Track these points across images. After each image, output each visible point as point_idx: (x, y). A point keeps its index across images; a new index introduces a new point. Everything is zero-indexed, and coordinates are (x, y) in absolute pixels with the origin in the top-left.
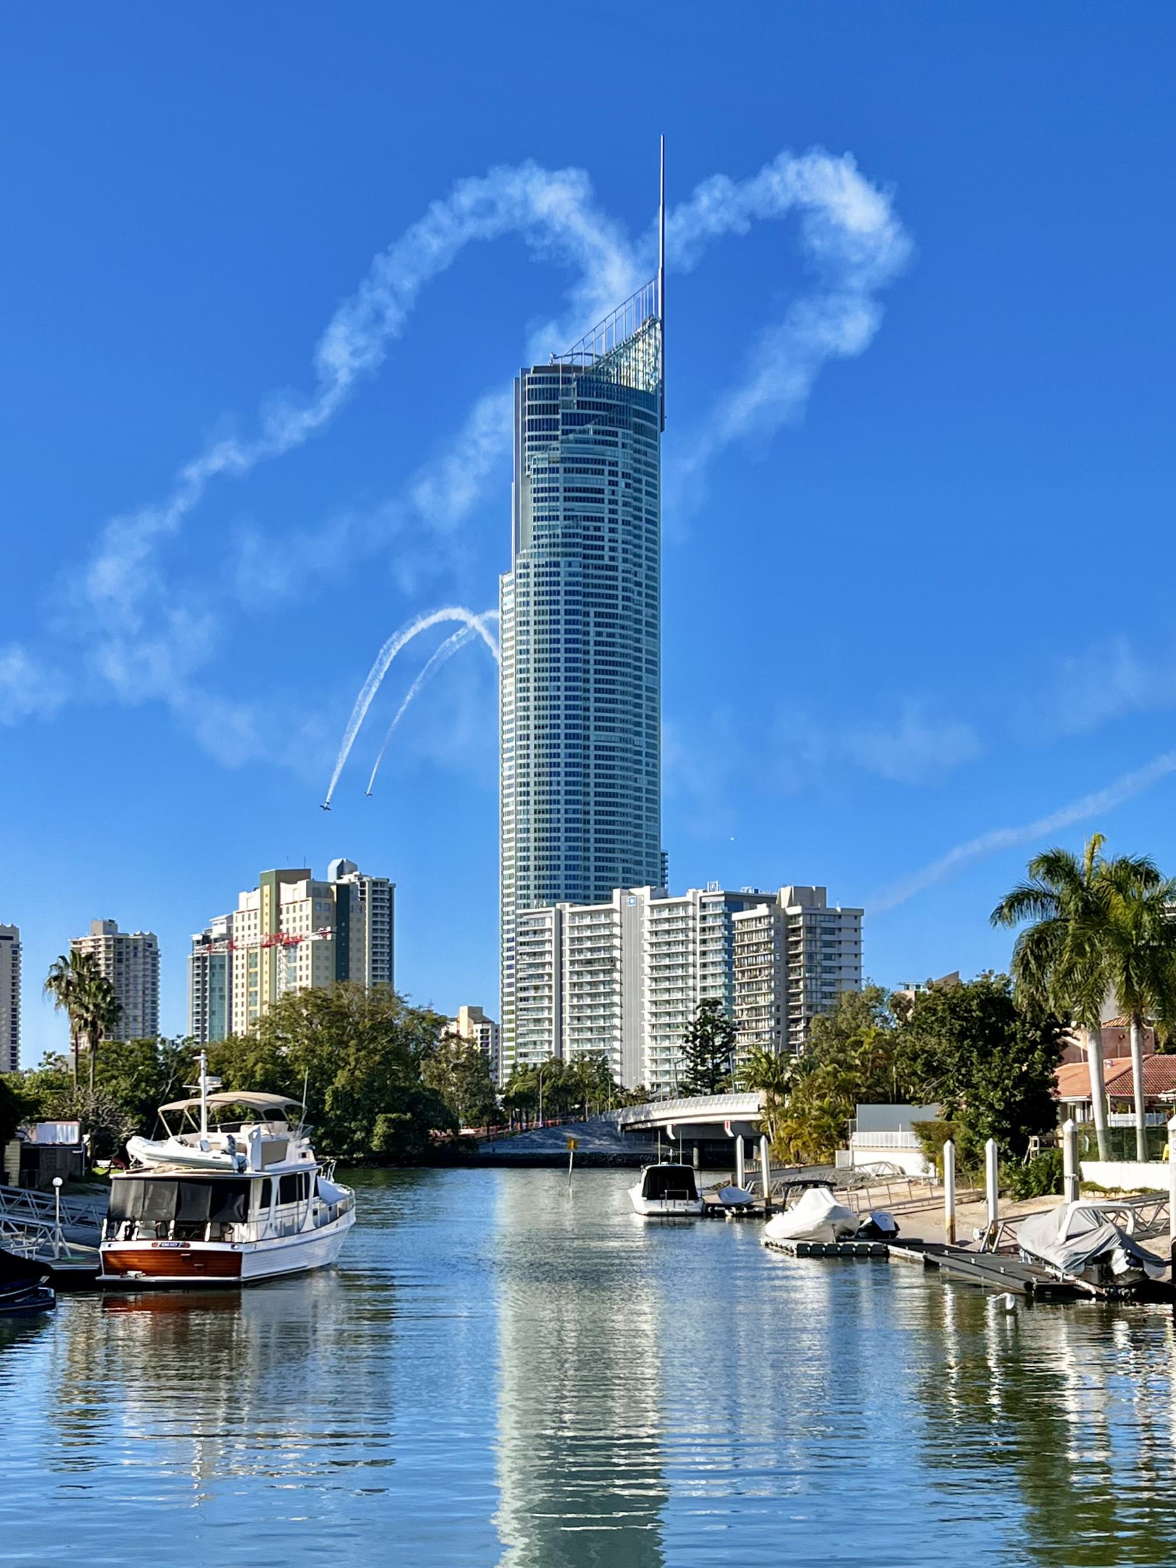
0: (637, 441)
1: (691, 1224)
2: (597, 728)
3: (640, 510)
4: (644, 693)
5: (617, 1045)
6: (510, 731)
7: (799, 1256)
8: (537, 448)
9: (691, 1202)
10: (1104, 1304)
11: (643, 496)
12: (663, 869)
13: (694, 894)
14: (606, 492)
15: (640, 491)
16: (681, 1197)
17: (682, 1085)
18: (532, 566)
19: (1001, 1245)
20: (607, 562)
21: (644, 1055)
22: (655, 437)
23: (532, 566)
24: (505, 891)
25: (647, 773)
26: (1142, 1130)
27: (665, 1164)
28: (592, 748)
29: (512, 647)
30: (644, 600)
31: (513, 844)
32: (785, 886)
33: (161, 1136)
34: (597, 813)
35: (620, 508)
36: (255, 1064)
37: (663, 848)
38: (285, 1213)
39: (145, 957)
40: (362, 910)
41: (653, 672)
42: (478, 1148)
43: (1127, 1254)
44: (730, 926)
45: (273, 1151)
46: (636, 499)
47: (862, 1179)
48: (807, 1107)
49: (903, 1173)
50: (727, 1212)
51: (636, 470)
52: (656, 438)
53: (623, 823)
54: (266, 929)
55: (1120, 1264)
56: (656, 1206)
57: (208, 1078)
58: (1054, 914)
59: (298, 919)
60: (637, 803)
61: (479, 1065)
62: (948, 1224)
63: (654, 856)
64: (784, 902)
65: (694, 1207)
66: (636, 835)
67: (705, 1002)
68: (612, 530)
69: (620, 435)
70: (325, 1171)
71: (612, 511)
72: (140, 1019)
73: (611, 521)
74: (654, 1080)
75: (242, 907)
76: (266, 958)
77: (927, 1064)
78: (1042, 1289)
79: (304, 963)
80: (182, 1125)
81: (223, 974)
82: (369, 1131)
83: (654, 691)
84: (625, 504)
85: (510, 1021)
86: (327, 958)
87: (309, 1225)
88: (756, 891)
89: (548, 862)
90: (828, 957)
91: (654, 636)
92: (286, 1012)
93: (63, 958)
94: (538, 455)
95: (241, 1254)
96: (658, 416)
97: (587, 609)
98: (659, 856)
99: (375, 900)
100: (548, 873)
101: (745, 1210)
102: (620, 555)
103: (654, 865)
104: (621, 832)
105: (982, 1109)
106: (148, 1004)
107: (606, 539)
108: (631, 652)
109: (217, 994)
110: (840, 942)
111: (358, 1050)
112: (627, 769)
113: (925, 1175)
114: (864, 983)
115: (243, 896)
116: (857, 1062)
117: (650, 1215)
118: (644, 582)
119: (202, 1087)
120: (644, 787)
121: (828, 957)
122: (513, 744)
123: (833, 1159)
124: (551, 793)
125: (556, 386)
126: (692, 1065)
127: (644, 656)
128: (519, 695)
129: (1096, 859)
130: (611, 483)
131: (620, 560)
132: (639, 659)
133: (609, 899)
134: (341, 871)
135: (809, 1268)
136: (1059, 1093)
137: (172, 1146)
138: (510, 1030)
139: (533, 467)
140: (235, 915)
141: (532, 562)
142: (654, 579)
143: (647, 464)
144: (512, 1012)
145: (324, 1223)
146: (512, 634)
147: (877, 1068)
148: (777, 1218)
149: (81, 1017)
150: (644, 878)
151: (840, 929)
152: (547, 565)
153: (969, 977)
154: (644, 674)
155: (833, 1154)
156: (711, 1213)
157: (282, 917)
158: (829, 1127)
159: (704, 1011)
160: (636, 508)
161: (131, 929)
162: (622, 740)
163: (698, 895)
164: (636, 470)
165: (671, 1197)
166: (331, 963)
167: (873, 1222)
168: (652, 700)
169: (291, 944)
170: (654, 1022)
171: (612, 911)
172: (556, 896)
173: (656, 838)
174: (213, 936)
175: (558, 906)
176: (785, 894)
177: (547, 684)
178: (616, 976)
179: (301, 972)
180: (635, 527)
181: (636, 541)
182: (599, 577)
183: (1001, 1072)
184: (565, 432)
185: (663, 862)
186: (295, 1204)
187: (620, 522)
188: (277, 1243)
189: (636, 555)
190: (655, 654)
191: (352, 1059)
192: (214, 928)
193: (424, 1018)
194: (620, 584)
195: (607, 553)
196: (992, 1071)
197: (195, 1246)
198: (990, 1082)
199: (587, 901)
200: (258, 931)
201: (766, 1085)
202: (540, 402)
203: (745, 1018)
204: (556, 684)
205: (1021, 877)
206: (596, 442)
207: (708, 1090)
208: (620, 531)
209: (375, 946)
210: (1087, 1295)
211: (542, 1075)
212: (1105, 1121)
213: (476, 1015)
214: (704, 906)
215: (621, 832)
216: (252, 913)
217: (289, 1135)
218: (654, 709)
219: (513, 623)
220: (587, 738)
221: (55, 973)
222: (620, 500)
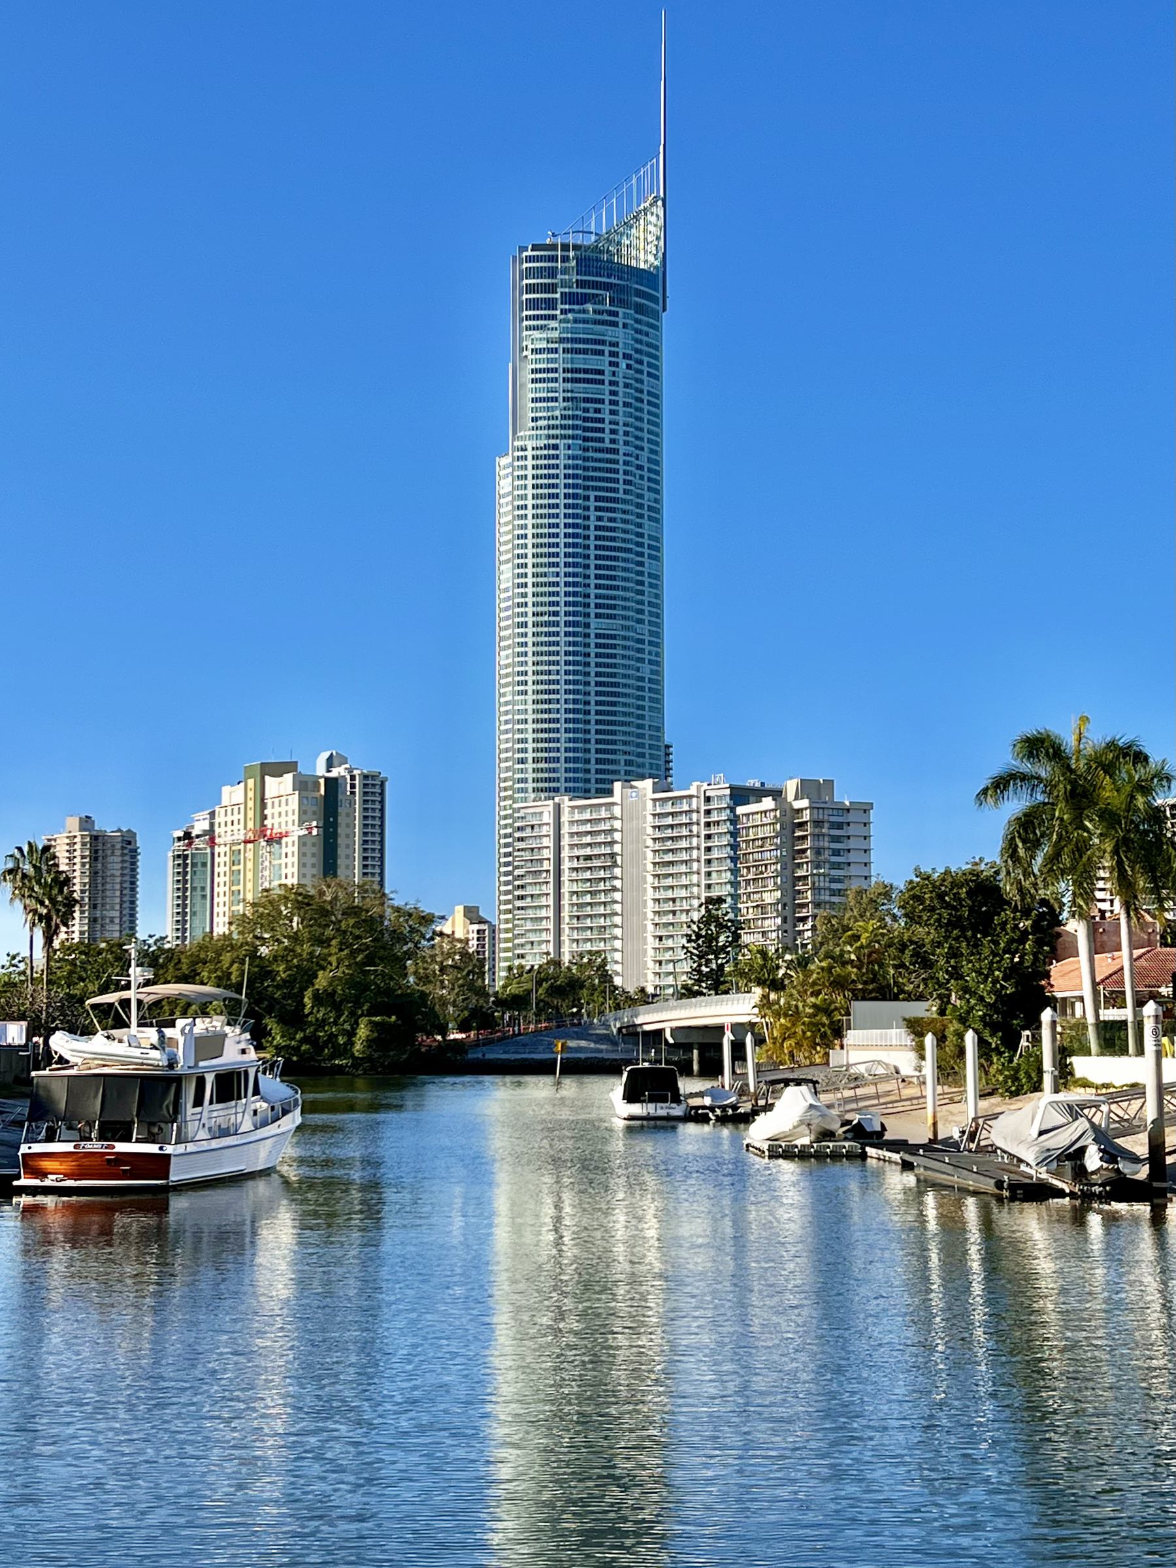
0: (637, 321)
1: (674, 1128)
2: (598, 616)
3: (641, 391)
4: (646, 579)
5: (618, 944)
6: (507, 618)
7: (770, 1157)
8: (535, 328)
9: (674, 1105)
10: (1078, 1203)
11: (645, 378)
12: (668, 762)
13: (698, 788)
14: (606, 373)
15: (641, 372)
17: (684, 987)
18: (529, 448)
19: (983, 1143)
20: (607, 445)
21: (643, 954)
22: (657, 317)
23: (529, 448)
25: (651, 662)
26: (1133, 1022)
27: (646, 1065)
28: (592, 636)
29: (509, 532)
30: (646, 483)
31: (510, 735)
32: (791, 778)
33: (87, 1031)
34: (598, 703)
35: (621, 389)
36: (231, 965)
37: (667, 740)
38: (221, 1113)
39: (123, 855)
40: (352, 803)
41: (656, 558)
42: (466, 1053)
43: (1100, 1150)
44: (734, 820)
45: (211, 1045)
46: (637, 380)
47: (856, 1079)
48: (800, 1005)
49: (897, 1072)
50: (711, 1115)
51: (637, 351)
52: (658, 318)
53: (625, 714)
54: (250, 825)
55: (1093, 1160)
56: (637, 1109)
57: (139, 969)
58: (1040, 798)
59: (283, 814)
60: (640, 693)
61: (472, 966)
62: (930, 1121)
63: (658, 748)
64: (790, 796)
65: (678, 1111)
66: (640, 726)
67: (709, 900)
68: (612, 412)
69: (620, 315)
70: (272, 1070)
71: (613, 393)
72: (117, 921)
73: (612, 402)
74: (657, 983)
75: (225, 801)
76: (250, 855)
77: (916, 954)
78: (1013, 1187)
79: (290, 860)
80: (114, 1018)
81: (205, 873)
82: (352, 1034)
83: (657, 577)
84: (626, 386)
85: (507, 921)
86: (314, 855)
87: (247, 1125)
88: (763, 784)
89: (546, 755)
90: (836, 853)
91: (657, 520)
92: (266, 912)
93: (20, 849)
94: (536, 334)
95: (169, 1156)
96: (660, 295)
97: (587, 493)
98: (663, 748)
99: (365, 793)
100: (546, 765)
101: (730, 1112)
102: (621, 438)
103: (658, 757)
104: (623, 724)
105: (973, 1002)
106: (127, 905)
107: (607, 421)
108: (632, 537)
109: (199, 892)
110: (849, 837)
111: (341, 950)
112: (629, 658)
113: (917, 1074)
114: (873, 879)
115: (226, 790)
116: (853, 957)
117: (631, 1118)
118: (646, 465)
119: (132, 979)
120: (647, 676)
121: (836, 853)
122: (510, 631)
123: (828, 1060)
124: (550, 682)
125: (554, 264)
126: (695, 965)
127: (646, 541)
128: (517, 581)
129: (1083, 740)
130: (611, 364)
131: (621, 443)
132: (641, 545)
133: (610, 792)
134: (330, 764)
135: (788, 1169)
136: (1052, 986)
137: (98, 1043)
138: (507, 931)
139: (530, 347)
140: (217, 810)
141: (530, 444)
142: (657, 463)
143: (648, 345)
144: (510, 911)
145: (264, 1124)
146: (510, 518)
147: (872, 959)
148: (761, 1119)
149: (35, 911)
150: (647, 771)
151: (848, 824)
152: (545, 447)
153: (960, 864)
154: (645, 560)
155: (827, 1054)
156: (697, 1117)
157: (266, 812)
158: (824, 1025)
159: (708, 911)
160: (637, 390)
161: (107, 825)
162: (624, 627)
163: (704, 788)
164: (637, 351)
165: (653, 1099)
166: (318, 860)
168: (655, 586)
169: (275, 840)
170: (657, 921)
171: (613, 804)
172: (556, 790)
173: (659, 729)
174: (194, 833)
175: (557, 800)
176: (791, 787)
177: (546, 570)
178: (617, 872)
179: (286, 868)
180: (637, 409)
181: (638, 424)
182: (600, 460)
183: (992, 963)
184: (563, 312)
185: (668, 754)
186: (233, 1103)
187: (621, 404)
188: (215, 1144)
189: (637, 438)
190: (657, 539)
191: (333, 959)
192: (196, 824)
193: (410, 915)
194: (621, 467)
195: (607, 436)
196: (981, 961)
197: (121, 1147)
198: (979, 972)
199: (588, 795)
200: (242, 826)
201: (760, 982)
202: (539, 281)
203: (750, 916)
204: (554, 569)
205: (1006, 759)
206: (595, 322)
207: (712, 992)
208: (621, 413)
209: (365, 842)
210: (1061, 1194)
211: (540, 976)
212: (1097, 1015)
213: (472, 915)
214: (708, 799)
215: (623, 724)
216: (236, 808)
217: (227, 1029)
219: (510, 507)
220: (587, 625)
221: (10, 865)
222: (621, 381)
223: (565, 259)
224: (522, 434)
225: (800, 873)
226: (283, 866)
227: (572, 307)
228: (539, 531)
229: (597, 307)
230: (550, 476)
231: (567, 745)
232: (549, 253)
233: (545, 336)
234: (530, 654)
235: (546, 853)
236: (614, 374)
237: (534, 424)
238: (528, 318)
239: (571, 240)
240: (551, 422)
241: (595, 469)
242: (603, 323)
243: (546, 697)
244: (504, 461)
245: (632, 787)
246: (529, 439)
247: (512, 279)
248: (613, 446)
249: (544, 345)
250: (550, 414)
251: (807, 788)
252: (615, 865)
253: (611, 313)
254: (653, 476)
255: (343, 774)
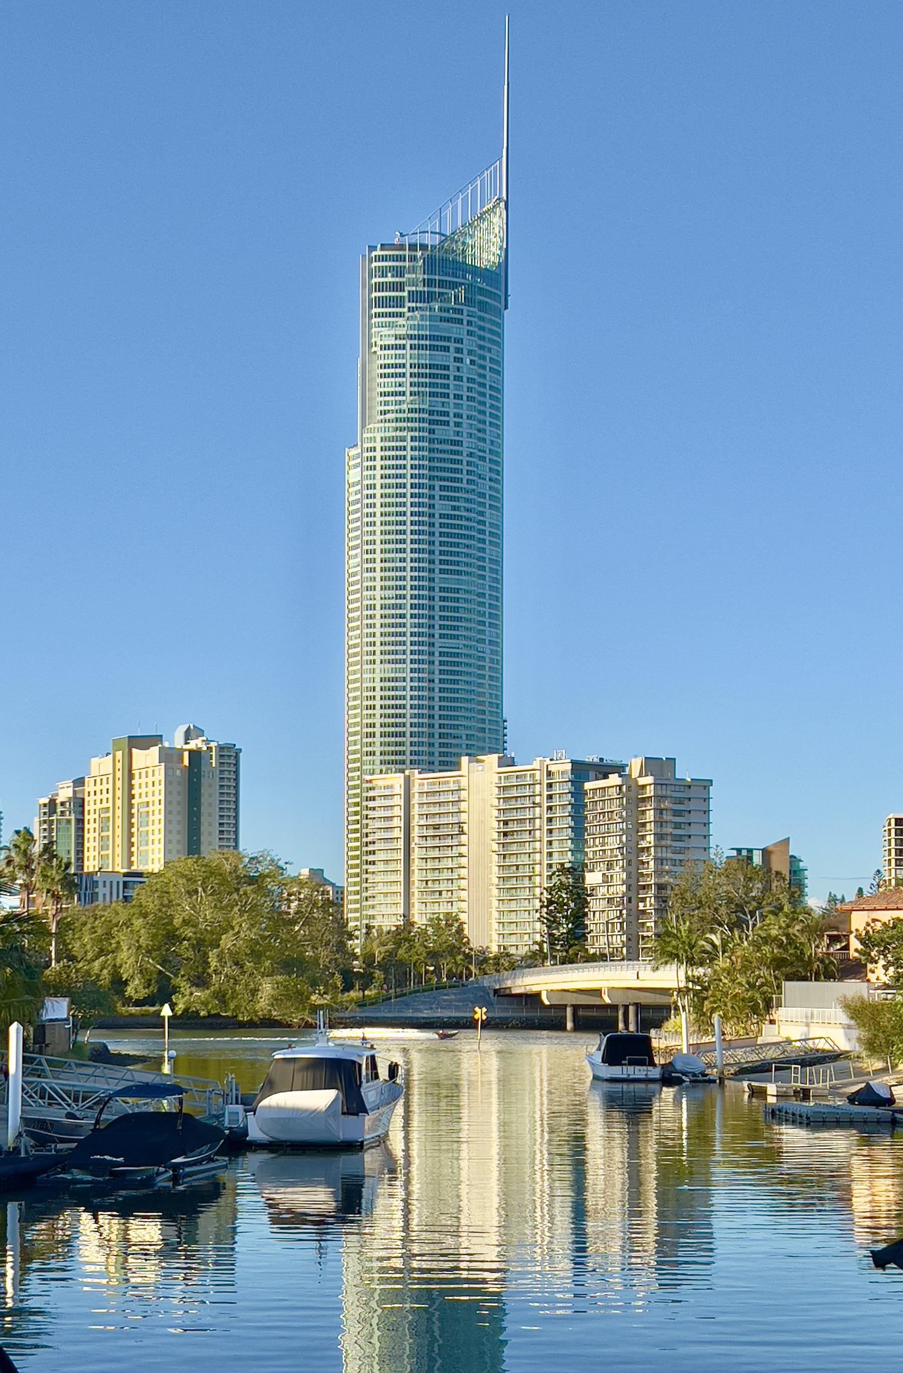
0: (481, 319)
2: (442, 636)
9: (650, 1068)
16: (641, 1063)
21: (496, 917)
22: (500, 315)
24: (350, 757)
32: (636, 757)
51: (481, 347)
65: (655, 1073)
68: (457, 406)
85: (355, 884)
94: (385, 331)
97: (432, 483)
115: (95, 761)
130: (456, 360)
133: (457, 766)
134: (188, 736)
139: (379, 343)
143: (491, 331)
157: (133, 792)
164: (481, 347)
165: (632, 1063)
167: (160, 1069)
168: (496, 571)
176: (635, 766)
181: (481, 417)
192: (60, 792)
199: (432, 767)
214: (549, 774)
216: (104, 778)
218: (496, 580)
223: (413, 259)
224: (372, 426)
225: (643, 844)
226: (150, 833)
227: (419, 305)
228: (387, 519)
229: (443, 305)
230: (397, 467)
231: (413, 720)
232: (397, 253)
233: (392, 332)
234: (378, 533)
235: (396, 822)
236: (458, 369)
237: (382, 417)
238: (378, 315)
239: (417, 239)
240: (399, 415)
241: (441, 460)
242: (448, 320)
243: (393, 648)
244: (354, 452)
245: (478, 761)
246: (376, 434)
247: (363, 276)
248: (457, 438)
249: (392, 341)
250: (397, 407)
251: (651, 765)
252: (462, 833)
253: (455, 311)
254: (494, 476)
255: (200, 746)
